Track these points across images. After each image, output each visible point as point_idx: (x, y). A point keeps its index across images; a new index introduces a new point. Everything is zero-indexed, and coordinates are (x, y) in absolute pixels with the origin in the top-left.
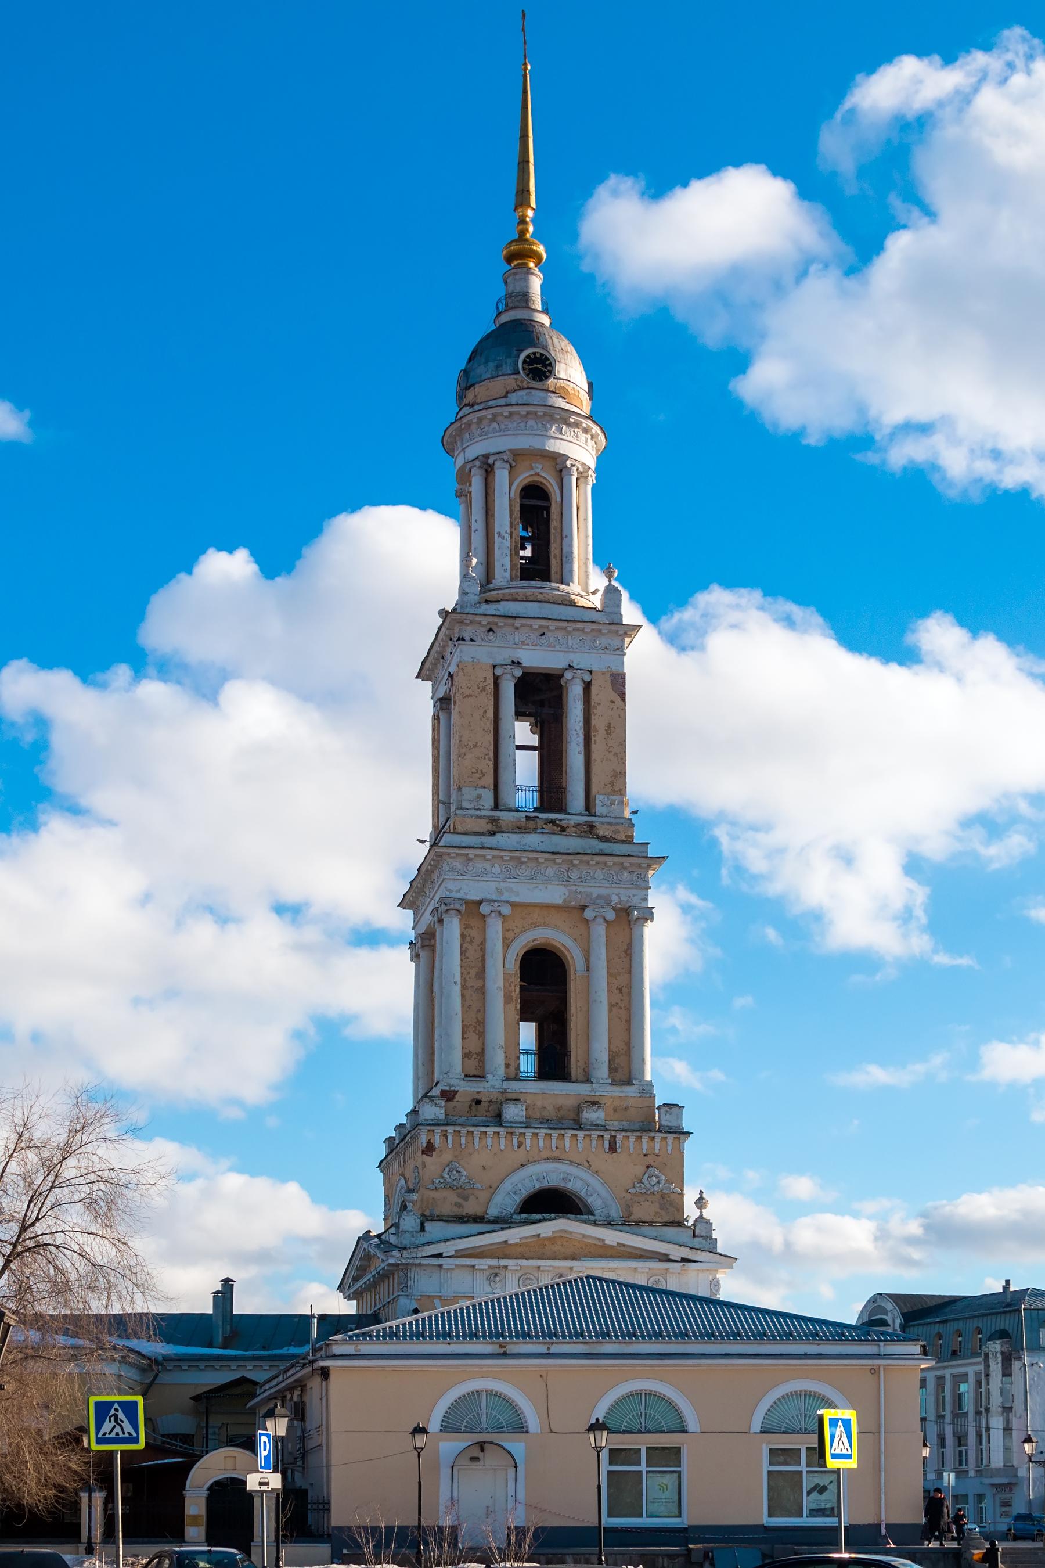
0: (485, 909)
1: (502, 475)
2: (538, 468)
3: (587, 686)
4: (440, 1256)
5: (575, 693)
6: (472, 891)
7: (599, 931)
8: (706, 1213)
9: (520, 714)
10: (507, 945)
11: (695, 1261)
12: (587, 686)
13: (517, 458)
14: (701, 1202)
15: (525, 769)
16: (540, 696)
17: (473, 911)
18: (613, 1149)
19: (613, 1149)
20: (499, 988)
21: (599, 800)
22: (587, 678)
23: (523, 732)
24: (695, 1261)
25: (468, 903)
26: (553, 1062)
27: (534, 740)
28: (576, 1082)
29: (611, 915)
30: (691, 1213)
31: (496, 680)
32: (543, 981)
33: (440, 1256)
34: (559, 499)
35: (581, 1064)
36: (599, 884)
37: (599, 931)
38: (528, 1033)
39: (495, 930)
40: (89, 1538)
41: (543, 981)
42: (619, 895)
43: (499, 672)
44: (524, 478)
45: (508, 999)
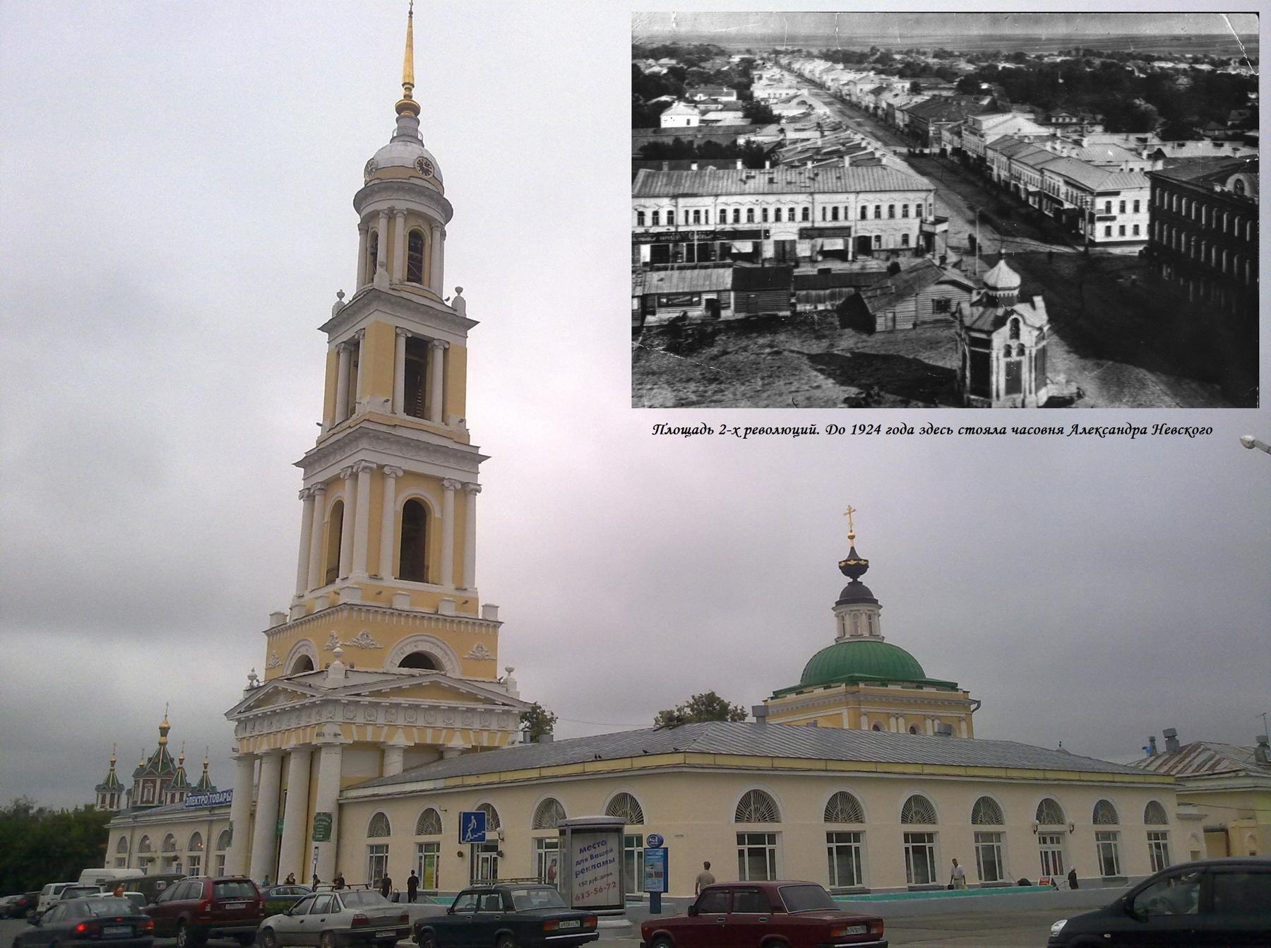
0: (386, 470)
1: (400, 221)
2: (421, 221)
3: (446, 350)
4: (358, 695)
5: (439, 354)
7: (450, 495)
12: (446, 350)
13: (411, 213)
14: (459, 290)
17: (379, 473)
29: (459, 486)
33: (358, 695)
37: (450, 495)
42: (464, 478)
43: (399, 331)
44: (414, 224)
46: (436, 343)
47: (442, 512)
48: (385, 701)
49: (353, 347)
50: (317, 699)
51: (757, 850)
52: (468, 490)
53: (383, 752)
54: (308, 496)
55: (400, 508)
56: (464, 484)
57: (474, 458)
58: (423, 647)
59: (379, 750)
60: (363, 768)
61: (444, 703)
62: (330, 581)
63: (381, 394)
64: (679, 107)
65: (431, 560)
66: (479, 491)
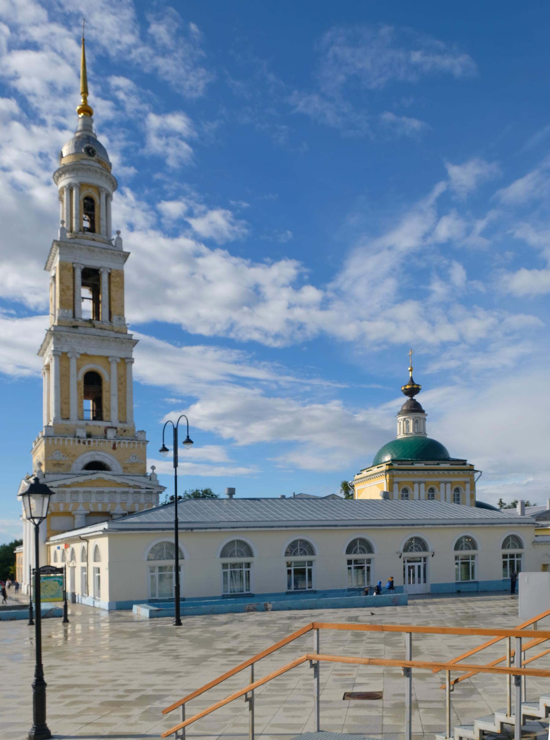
2: (90, 190)
5: (104, 278)
7: (114, 367)
8: (155, 471)
9: (84, 285)
10: (78, 369)
11: (75, 676)
12: (110, 274)
14: (153, 468)
15: (87, 306)
16: (91, 277)
18: (114, 448)
19: (114, 448)
20: (428, 623)
21: (115, 318)
22: (109, 271)
23: (86, 292)
24: (75, 676)
25: (63, 353)
26: (98, 415)
27: (91, 296)
28: (106, 421)
29: (119, 360)
30: (149, 471)
31: (74, 269)
32: (93, 383)
34: (99, 203)
35: (483, 611)
36: (114, 352)
37: (114, 367)
38: (89, 404)
39: (73, 364)
40: (301, 618)
41: (93, 383)
43: (75, 265)
44: (85, 193)
45: (99, 218)
55: (81, 378)
56: (123, 359)
58: (98, 458)
66: (132, 362)
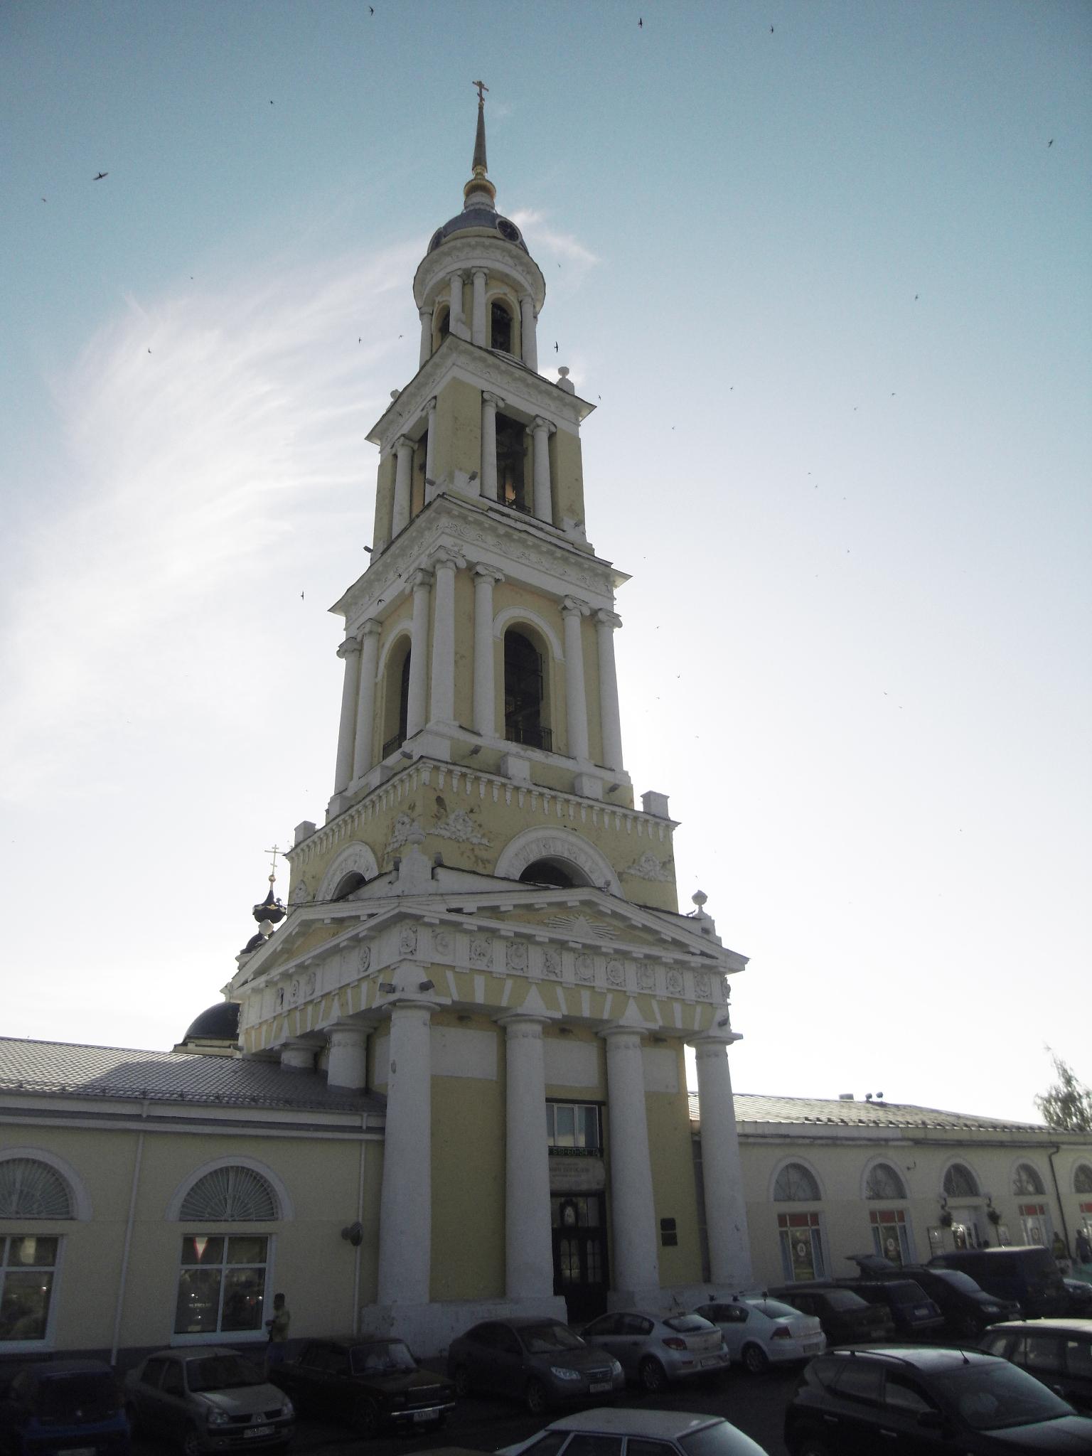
2: (507, 290)
4: (459, 911)
6: (473, 554)
7: (574, 623)
12: (552, 436)
13: (491, 276)
22: (553, 429)
33: (459, 911)
37: (574, 623)
42: (596, 603)
44: (498, 291)
46: (539, 421)
47: (563, 650)
48: (507, 928)
49: (421, 441)
50: (447, 834)
51: (371, 1291)
52: (600, 622)
53: (503, 1033)
54: (351, 649)
55: (501, 637)
56: (595, 613)
57: (606, 576)
59: (496, 1022)
60: (471, 1053)
61: (639, 951)
62: (388, 750)
63: (469, 468)
64: (268, 1015)
65: (554, 716)
